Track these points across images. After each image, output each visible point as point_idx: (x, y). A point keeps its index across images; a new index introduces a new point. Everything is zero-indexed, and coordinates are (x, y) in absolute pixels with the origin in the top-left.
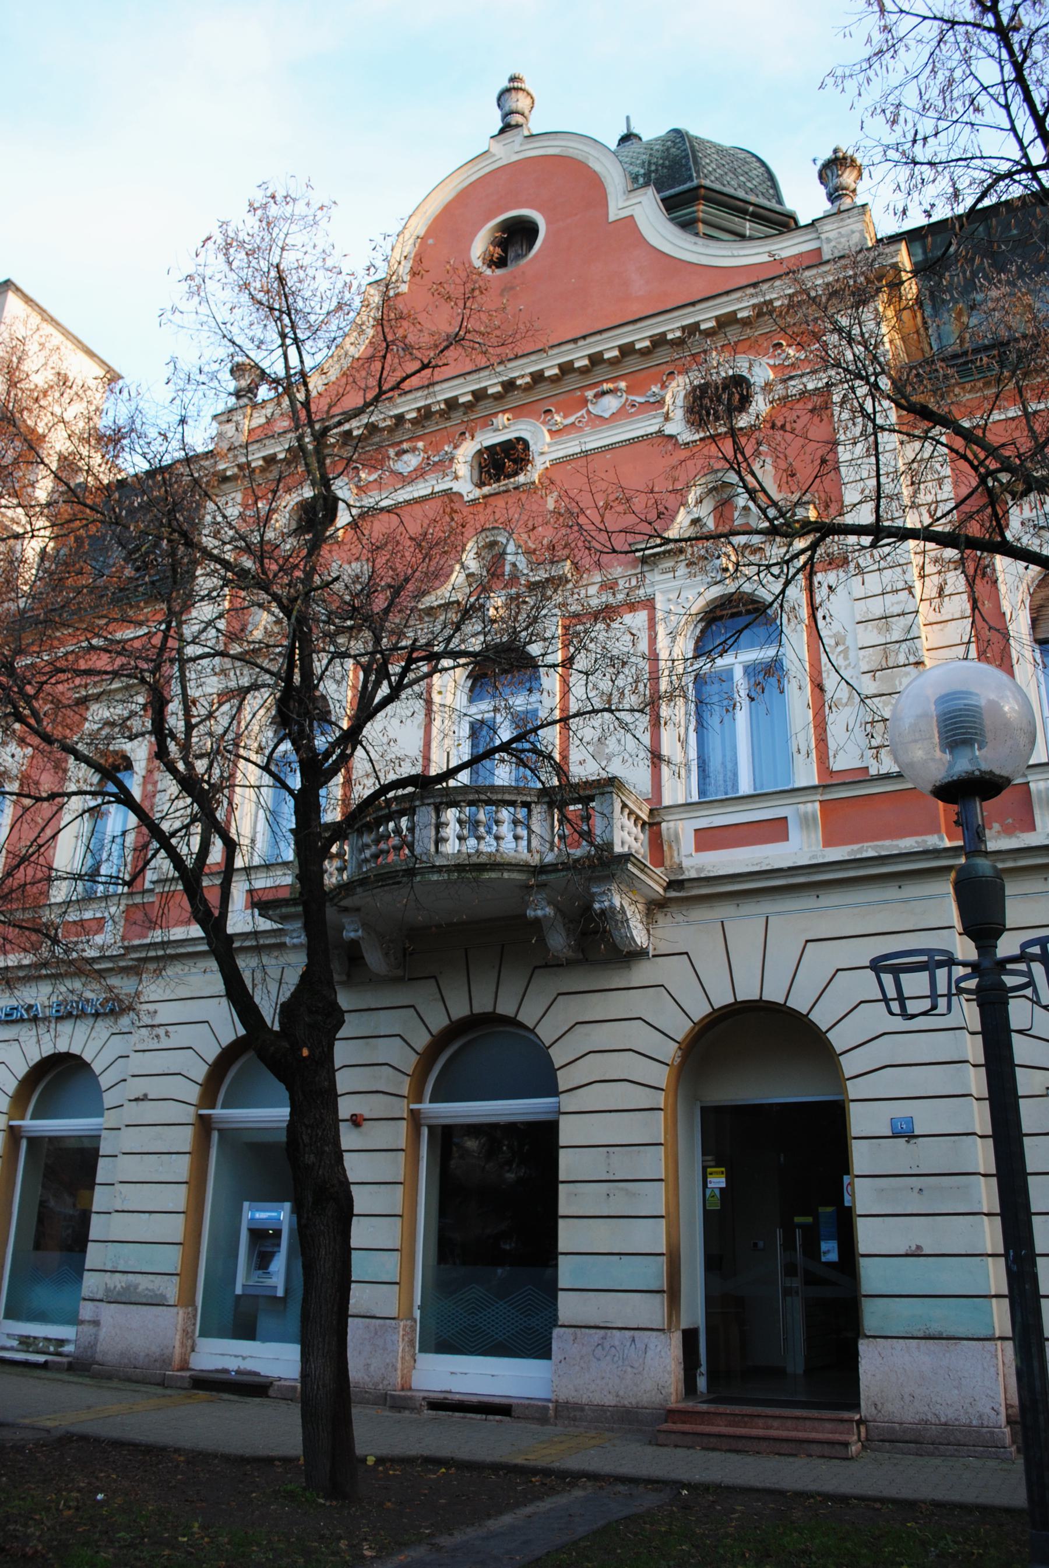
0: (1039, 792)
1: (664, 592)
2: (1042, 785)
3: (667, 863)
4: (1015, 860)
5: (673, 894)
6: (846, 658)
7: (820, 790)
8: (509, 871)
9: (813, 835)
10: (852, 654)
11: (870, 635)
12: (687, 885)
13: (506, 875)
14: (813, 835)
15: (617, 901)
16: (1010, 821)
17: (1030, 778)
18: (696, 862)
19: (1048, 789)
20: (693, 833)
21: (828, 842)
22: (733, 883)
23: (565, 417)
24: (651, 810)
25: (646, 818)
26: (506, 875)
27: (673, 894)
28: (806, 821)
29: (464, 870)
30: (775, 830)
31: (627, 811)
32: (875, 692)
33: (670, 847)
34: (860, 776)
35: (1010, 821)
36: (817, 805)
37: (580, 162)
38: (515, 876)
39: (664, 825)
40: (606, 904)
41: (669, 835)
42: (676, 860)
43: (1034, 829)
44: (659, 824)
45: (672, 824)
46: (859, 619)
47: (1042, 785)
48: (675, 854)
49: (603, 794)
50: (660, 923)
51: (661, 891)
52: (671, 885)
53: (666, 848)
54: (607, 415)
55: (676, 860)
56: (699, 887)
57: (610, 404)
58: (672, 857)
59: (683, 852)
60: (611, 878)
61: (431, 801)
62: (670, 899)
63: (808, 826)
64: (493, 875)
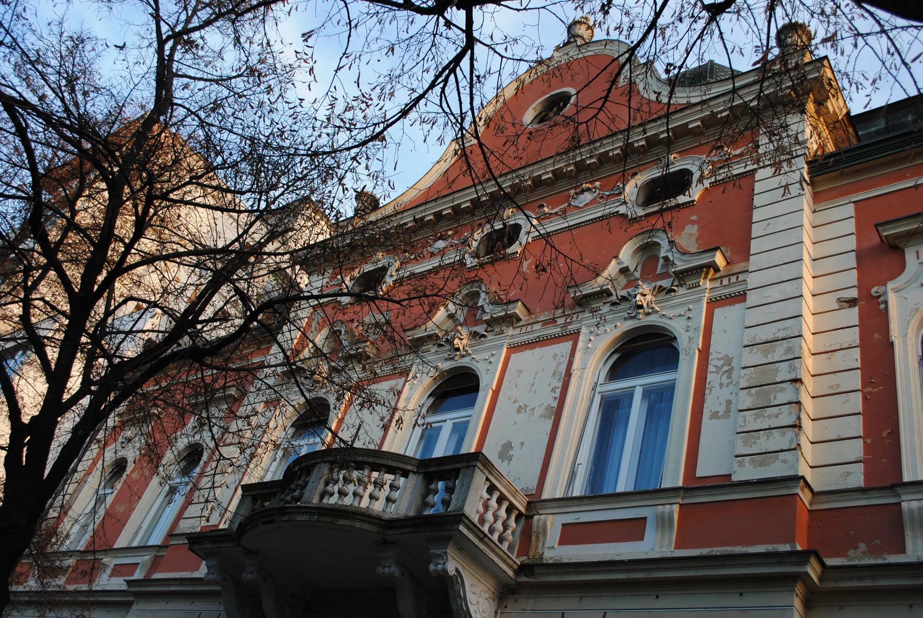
0: (911, 511)
1: (588, 326)
2: (915, 505)
3: (532, 553)
4: (874, 579)
5: (524, 579)
6: (729, 377)
7: (681, 493)
8: (362, 521)
9: (667, 537)
10: (735, 375)
11: (754, 357)
12: (536, 571)
13: (358, 525)
14: (667, 537)
15: (451, 568)
16: (878, 541)
17: (903, 498)
18: (553, 549)
19: (922, 509)
20: (560, 527)
21: (678, 547)
22: (577, 573)
23: (552, 209)
24: (529, 503)
25: (523, 510)
26: (358, 525)
27: (524, 579)
28: (663, 522)
29: (324, 515)
30: (633, 529)
31: (496, 496)
32: (750, 405)
33: (538, 539)
34: (723, 483)
35: (878, 541)
36: (676, 508)
37: (894, 278)
38: (366, 526)
39: (536, 517)
40: (440, 567)
41: (538, 526)
42: (540, 551)
43: (905, 552)
44: (532, 517)
45: (543, 516)
46: (746, 343)
47: (915, 505)
48: (540, 546)
49: (467, 467)
50: (509, 610)
51: (510, 573)
52: (523, 569)
53: (533, 539)
54: (581, 205)
55: (540, 551)
56: (548, 574)
57: (587, 197)
58: (537, 547)
59: (548, 543)
60: (445, 540)
61: (329, 459)
62: (521, 585)
63: (663, 527)
64: (347, 523)
